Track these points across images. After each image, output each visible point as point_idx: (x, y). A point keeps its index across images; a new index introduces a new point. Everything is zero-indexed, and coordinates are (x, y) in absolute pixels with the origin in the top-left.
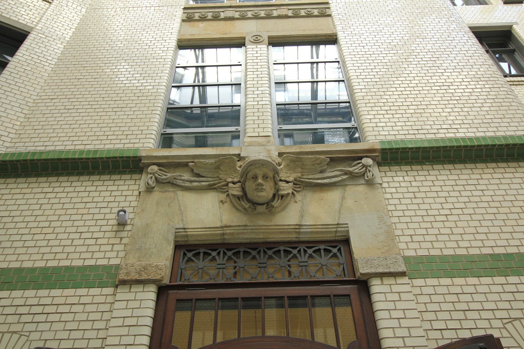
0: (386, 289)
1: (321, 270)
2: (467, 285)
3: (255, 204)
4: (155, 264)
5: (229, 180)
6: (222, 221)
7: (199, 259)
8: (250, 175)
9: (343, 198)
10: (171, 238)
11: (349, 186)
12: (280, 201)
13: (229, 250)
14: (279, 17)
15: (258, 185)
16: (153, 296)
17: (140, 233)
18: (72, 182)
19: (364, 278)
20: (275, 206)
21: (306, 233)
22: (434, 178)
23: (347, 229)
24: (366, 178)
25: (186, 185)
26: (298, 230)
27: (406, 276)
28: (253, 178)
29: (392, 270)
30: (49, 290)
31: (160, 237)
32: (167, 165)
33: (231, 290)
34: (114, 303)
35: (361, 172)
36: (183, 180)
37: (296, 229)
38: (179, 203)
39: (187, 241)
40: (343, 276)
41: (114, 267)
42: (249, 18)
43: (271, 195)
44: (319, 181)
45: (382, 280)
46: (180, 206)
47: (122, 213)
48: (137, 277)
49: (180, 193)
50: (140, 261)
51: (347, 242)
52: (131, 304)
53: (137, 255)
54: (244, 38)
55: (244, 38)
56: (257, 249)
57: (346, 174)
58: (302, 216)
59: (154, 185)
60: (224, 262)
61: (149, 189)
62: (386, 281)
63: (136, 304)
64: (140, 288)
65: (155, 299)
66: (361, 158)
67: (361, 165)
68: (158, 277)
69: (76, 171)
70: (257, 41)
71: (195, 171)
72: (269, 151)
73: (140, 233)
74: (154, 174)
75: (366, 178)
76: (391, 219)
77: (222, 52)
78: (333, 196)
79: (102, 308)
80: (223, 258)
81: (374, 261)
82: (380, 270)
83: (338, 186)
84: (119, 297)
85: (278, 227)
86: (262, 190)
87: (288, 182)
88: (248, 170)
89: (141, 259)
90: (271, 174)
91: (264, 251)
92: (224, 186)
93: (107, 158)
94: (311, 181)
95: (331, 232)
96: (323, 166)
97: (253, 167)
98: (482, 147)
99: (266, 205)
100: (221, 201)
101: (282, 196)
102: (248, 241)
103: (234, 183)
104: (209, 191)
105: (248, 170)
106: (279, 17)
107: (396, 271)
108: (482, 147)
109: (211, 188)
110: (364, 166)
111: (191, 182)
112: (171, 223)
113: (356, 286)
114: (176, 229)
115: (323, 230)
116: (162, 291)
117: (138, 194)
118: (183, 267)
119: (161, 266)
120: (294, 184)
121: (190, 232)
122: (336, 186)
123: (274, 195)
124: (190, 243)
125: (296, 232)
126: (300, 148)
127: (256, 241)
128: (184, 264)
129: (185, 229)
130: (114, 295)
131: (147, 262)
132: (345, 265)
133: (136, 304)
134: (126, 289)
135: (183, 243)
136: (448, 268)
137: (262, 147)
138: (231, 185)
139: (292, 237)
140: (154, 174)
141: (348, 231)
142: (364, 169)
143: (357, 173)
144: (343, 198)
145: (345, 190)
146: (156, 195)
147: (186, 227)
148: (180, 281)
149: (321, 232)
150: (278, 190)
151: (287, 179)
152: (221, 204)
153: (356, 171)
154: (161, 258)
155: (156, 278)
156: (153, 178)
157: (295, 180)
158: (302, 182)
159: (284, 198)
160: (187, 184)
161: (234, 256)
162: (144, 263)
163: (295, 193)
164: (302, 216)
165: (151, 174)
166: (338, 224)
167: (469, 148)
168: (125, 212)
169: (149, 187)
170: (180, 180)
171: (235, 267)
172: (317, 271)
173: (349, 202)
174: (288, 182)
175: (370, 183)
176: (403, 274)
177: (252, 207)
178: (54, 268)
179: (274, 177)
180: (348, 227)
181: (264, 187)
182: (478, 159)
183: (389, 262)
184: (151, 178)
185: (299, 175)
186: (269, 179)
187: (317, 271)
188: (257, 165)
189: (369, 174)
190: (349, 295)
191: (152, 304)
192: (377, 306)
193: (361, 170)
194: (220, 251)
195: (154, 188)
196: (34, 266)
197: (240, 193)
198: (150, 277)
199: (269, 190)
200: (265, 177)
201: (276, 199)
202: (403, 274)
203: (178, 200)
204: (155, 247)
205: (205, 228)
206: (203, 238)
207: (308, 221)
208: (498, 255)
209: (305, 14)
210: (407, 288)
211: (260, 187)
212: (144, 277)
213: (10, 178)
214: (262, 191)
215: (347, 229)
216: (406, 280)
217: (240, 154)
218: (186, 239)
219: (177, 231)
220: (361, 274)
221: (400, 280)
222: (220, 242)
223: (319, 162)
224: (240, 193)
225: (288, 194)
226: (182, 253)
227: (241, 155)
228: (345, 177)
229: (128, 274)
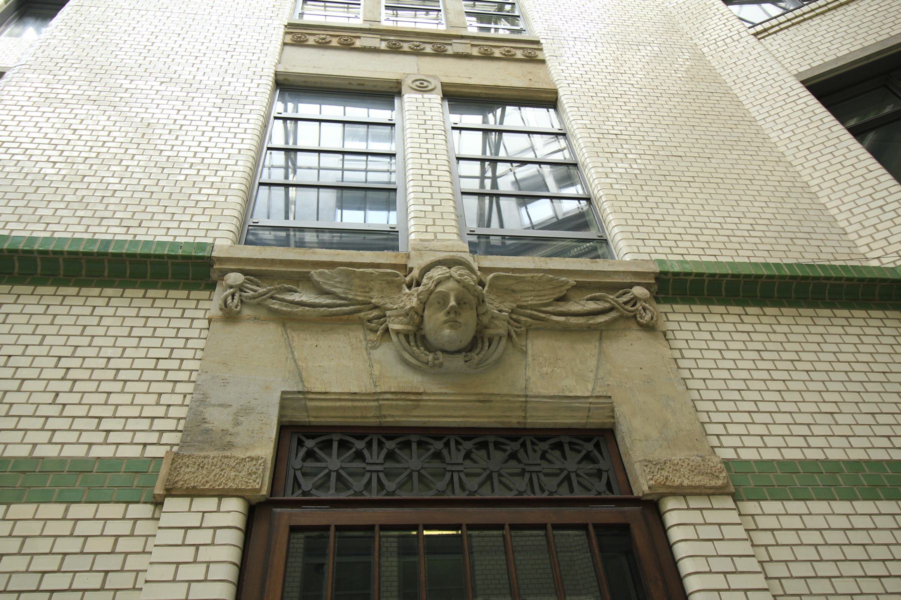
0: (694, 517)
1: (489, 483)
2: (787, 514)
7: (330, 455)
13: (389, 438)
14: (364, 50)
18: (65, 296)
19: (655, 498)
22: (712, 327)
30: (36, 505)
40: (529, 491)
42: (405, 53)
54: (399, 83)
55: (399, 83)
56: (519, 438)
60: (461, 461)
69: (161, 281)
70: (422, 88)
76: (722, 394)
77: (528, 112)
80: (379, 454)
91: (457, 443)
93: (55, 252)
98: (740, 279)
106: (364, 50)
108: (843, 282)
129: (526, 396)
136: (820, 483)
148: (293, 493)
161: (320, 449)
165: (231, 287)
167: (752, 279)
172: (481, 485)
178: (75, 460)
182: (678, 297)
187: (481, 485)
194: (449, 440)
195: (239, 312)
196: (62, 455)
208: (792, 462)
209: (314, 43)
213: (68, 286)
217: (406, 265)
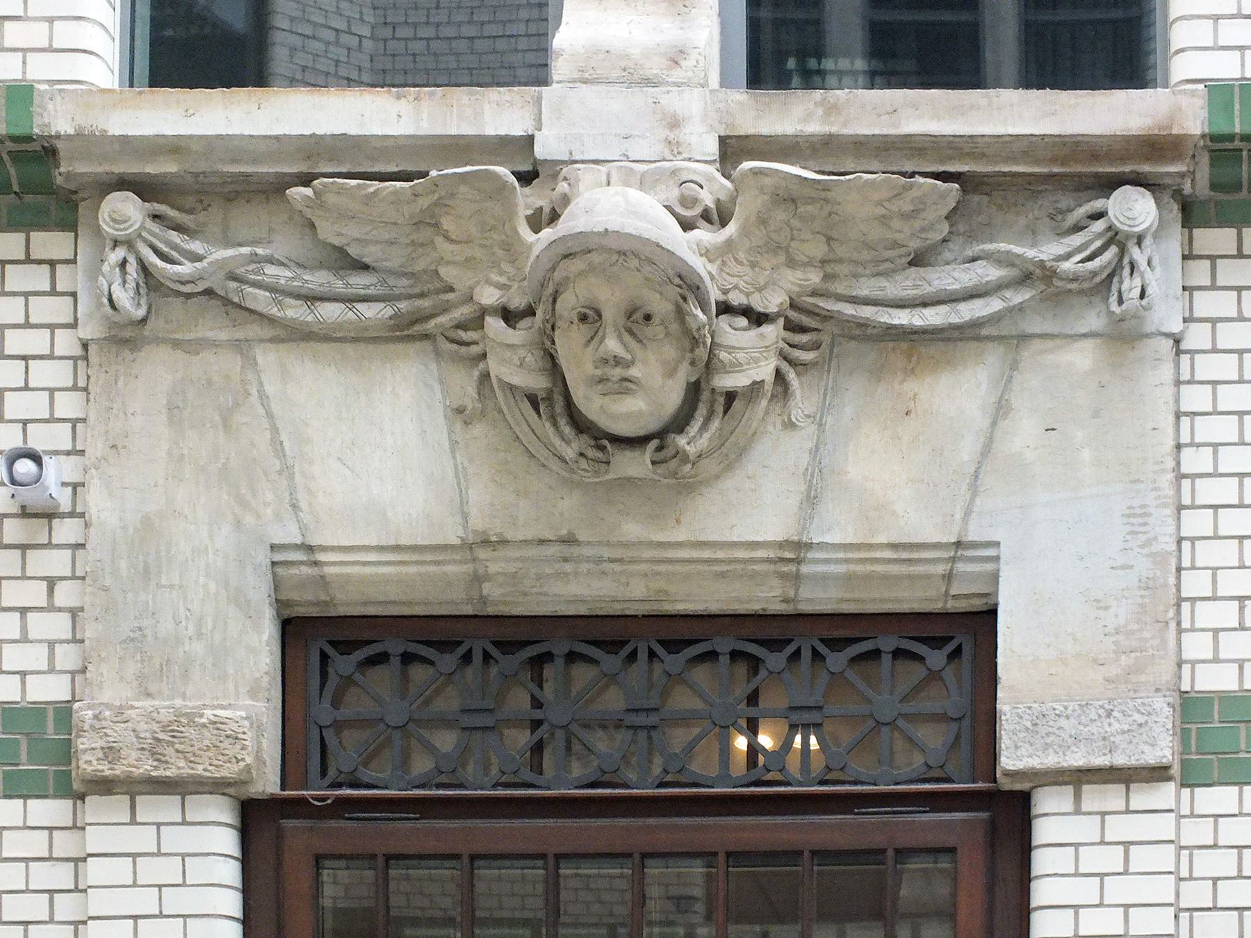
0: (1085, 828)
3: (606, 442)
4: (209, 713)
5: (489, 296)
6: (465, 516)
8: (568, 303)
9: (1001, 410)
10: (260, 593)
11: (1037, 345)
12: (715, 424)
15: (606, 361)
16: (227, 841)
17: (123, 564)
20: (691, 450)
21: (824, 578)
23: (989, 567)
24: (1115, 307)
25: (290, 313)
26: (792, 568)
27: (1169, 779)
28: (583, 318)
29: (1120, 760)
31: (212, 586)
32: (184, 190)
33: (516, 823)
34: (84, 860)
35: (1094, 274)
36: (272, 289)
37: (782, 560)
38: (270, 415)
39: (326, 603)
41: (51, 714)
43: (673, 397)
44: (902, 318)
45: (1078, 797)
46: (275, 430)
47: (25, 467)
48: (147, 767)
49: (267, 357)
50: (149, 695)
51: (984, 620)
52: (152, 870)
53: (132, 668)
56: (623, 643)
57: (1025, 279)
58: (811, 500)
59: (141, 313)
61: (125, 337)
62: (1098, 797)
63: (167, 870)
64: (164, 808)
65: (235, 850)
66: (1110, 184)
67: (1099, 226)
68: (229, 771)
71: (322, 235)
72: (674, 123)
73: (123, 564)
74: (129, 244)
75: (1115, 307)
78: (958, 394)
79: (44, 876)
81: (1062, 722)
82: (1077, 759)
83: (989, 338)
84: (96, 839)
85: (706, 554)
86: (626, 385)
87: (758, 319)
88: (558, 276)
89: (153, 688)
90: (660, 305)
92: (461, 326)
94: (867, 312)
95: (928, 577)
96: (931, 227)
97: (577, 265)
99: (654, 443)
100: (460, 411)
101: (731, 397)
102: (583, 610)
103: (509, 316)
104: (399, 347)
105: (558, 276)
107: (1133, 762)
109: (406, 331)
110: (1115, 238)
111: (312, 298)
112: (249, 520)
113: (984, 815)
114: (273, 547)
115: (894, 569)
116: (256, 819)
117: (78, 351)
118: (326, 720)
119: (234, 726)
120: (791, 327)
121: (334, 566)
122: (978, 338)
123: (694, 391)
124: (342, 611)
125: (783, 576)
126: (832, 110)
127: (617, 609)
128: (326, 704)
129: (310, 549)
130: (77, 827)
131: (178, 702)
132: (966, 723)
133: (167, 870)
134: (116, 806)
135: (314, 612)
137: (640, 98)
138: (494, 325)
139: (766, 597)
140: (129, 244)
141: (995, 577)
142: (1113, 250)
143: (1075, 279)
144: (1001, 410)
145: (1014, 366)
146: (157, 371)
147: (314, 541)
149: (885, 577)
150: (710, 366)
151: (758, 304)
152: (458, 426)
153: (1067, 266)
154: (231, 686)
155: (224, 773)
156: (132, 268)
157: (793, 306)
158: (827, 317)
159: (737, 405)
160: (295, 311)
162: (164, 706)
163: (791, 375)
164: (811, 500)
165: (116, 243)
166: (958, 544)
168: (36, 458)
169: (117, 318)
170: (255, 284)
171: (536, 724)
173: (1023, 434)
174: (758, 319)
175: (1125, 336)
176: (1158, 773)
177: (591, 453)
179: (681, 314)
180: (997, 559)
181: (634, 372)
183: (1116, 726)
184: (123, 264)
185: (815, 278)
186: (655, 329)
188: (595, 258)
189: (1125, 287)
190: (952, 850)
191: (231, 872)
192: (1041, 893)
193: (1090, 265)
197: (538, 383)
198: (199, 770)
199: (658, 380)
200: (638, 316)
201: (702, 410)
202: (1158, 773)
203: (263, 396)
204: (200, 635)
205: (397, 548)
206: (393, 593)
207: (836, 528)
210: (1163, 827)
211: (617, 372)
212: (176, 768)
214: (627, 392)
215: (989, 567)
216: (1164, 795)
217: (530, 140)
218: (323, 597)
219: (278, 557)
220: (1007, 774)
221: (1144, 797)
222: (468, 610)
223: (908, 207)
224: (538, 383)
225: (757, 386)
226: (315, 659)
227: (540, 151)
228: (1018, 297)
229: (110, 753)
